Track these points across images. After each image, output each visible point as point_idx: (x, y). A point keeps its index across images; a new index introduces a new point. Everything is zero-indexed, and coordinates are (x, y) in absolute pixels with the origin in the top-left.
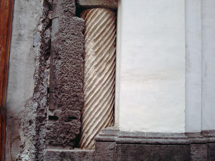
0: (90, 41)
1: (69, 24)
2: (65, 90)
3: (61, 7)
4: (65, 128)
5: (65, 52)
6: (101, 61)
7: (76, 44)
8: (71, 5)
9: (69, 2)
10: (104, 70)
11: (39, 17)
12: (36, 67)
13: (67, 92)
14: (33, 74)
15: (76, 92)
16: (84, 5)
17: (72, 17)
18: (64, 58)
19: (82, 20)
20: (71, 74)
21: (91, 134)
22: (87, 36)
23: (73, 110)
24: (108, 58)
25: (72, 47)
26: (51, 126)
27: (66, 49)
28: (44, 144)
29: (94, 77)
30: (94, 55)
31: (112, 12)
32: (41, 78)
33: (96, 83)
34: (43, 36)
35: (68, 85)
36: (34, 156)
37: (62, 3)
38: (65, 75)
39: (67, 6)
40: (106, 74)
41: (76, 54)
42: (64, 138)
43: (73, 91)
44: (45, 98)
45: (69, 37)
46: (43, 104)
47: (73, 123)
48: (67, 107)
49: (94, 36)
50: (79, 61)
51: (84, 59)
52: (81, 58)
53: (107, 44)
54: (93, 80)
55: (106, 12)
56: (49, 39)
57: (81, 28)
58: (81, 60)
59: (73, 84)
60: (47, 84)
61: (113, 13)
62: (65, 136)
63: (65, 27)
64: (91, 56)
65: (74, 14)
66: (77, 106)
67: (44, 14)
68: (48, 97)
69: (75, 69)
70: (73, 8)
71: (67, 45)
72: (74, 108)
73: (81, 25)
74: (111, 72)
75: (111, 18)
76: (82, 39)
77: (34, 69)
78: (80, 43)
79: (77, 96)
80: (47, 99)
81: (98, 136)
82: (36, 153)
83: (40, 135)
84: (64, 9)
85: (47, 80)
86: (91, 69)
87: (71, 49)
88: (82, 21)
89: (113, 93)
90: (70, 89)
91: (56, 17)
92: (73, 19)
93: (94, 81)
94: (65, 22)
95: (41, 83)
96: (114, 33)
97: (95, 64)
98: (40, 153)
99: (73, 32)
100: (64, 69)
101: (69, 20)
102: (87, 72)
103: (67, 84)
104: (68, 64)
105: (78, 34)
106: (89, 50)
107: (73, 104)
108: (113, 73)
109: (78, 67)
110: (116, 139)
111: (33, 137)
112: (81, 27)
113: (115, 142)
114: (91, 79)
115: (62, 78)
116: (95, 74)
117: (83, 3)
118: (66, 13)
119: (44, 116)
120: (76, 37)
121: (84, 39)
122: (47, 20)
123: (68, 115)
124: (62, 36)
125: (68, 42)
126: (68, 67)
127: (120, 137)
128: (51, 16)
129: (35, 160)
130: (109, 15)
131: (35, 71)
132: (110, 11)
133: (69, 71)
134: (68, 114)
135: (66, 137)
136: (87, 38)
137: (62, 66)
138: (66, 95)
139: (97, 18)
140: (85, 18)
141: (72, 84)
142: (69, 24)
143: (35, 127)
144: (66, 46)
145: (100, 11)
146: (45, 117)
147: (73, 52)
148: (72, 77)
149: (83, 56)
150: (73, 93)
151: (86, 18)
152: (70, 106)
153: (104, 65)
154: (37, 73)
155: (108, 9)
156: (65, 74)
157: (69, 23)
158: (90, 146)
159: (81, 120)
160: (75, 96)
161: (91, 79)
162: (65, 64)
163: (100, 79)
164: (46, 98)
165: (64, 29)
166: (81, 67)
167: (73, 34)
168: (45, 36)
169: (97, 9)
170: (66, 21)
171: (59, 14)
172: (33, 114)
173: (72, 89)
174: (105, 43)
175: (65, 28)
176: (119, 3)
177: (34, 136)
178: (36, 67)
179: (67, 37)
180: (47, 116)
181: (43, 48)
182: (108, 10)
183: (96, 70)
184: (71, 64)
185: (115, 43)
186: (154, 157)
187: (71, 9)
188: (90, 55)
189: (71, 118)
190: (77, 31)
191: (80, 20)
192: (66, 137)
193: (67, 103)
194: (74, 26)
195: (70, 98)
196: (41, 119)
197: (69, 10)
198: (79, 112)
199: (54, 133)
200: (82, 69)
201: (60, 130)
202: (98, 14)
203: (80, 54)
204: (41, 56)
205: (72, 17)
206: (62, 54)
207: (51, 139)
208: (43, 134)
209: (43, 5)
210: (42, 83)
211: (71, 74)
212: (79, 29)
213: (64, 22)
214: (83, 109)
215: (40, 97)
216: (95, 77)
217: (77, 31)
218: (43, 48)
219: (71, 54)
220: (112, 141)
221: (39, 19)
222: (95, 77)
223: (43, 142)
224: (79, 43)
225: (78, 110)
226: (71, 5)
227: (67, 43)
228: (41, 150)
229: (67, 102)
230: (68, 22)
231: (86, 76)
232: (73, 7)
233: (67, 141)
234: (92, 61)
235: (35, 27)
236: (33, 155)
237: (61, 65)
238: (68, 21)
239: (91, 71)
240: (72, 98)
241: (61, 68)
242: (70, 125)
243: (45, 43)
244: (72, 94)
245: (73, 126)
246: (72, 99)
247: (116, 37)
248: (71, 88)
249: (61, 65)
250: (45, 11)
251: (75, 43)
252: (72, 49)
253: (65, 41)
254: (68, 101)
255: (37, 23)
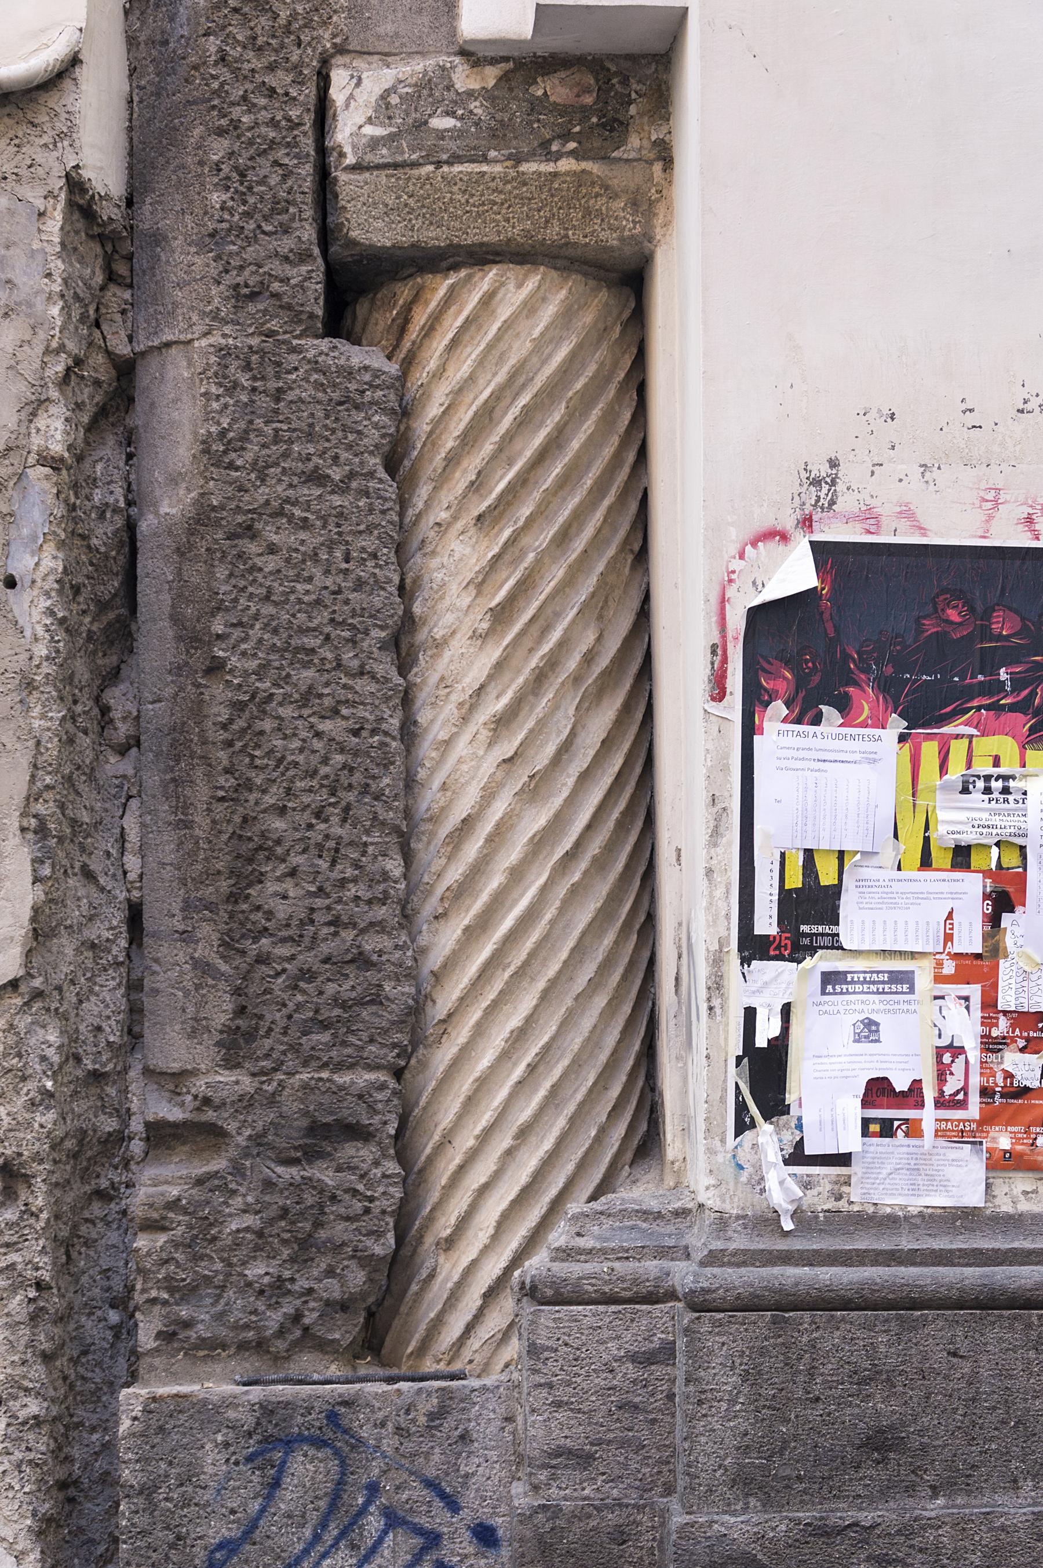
0: (449, 525)
1: (278, 395)
2: (269, 915)
3: (202, 263)
4: (285, 1211)
5: (256, 617)
6: (540, 678)
7: (338, 554)
8: (286, 244)
9: (266, 218)
10: (566, 748)
11: (39, 349)
12: (38, 743)
13: (284, 933)
14: (19, 799)
15: (354, 925)
16: (388, 244)
17: (295, 342)
18: (253, 664)
19: (376, 365)
20: (310, 790)
21: (486, 1250)
22: (424, 491)
23: (340, 1067)
24: (589, 658)
25: (310, 579)
26: (173, 1205)
27: (267, 598)
28: (112, 1345)
29: (489, 805)
30: (482, 638)
31: (603, 295)
32: (74, 822)
33: (512, 855)
34: (72, 499)
35: (293, 873)
36: (41, 1443)
37: (211, 226)
38: (269, 800)
39: (251, 253)
40: (585, 777)
41: (347, 634)
42: (279, 1287)
43: (329, 924)
44: (112, 984)
45: (287, 500)
46: (99, 1029)
47: (339, 1170)
48: (294, 1048)
49: (477, 486)
50: (372, 687)
51: (403, 669)
52: (385, 666)
53: (579, 544)
54: (486, 827)
55: (564, 292)
56: (119, 521)
57: (376, 426)
58: (387, 680)
59: (334, 863)
60: (125, 873)
61: (612, 302)
62: (287, 1274)
63: (251, 422)
64: (459, 645)
65: (312, 316)
66: (372, 1041)
67: (76, 315)
68: (133, 976)
69: (342, 751)
70: (304, 269)
71: (271, 563)
72: (349, 1051)
73: (377, 403)
74: (617, 762)
75: (600, 340)
76: (383, 512)
77: (24, 761)
78: (369, 543)
79: (362, 961)
80: (127, 995)
81: (537, 1263)
82: (55, 1419)
83: (85, 1279)
84: (228, 280)
85: (122, 838)
86: (461, 748)
87: (306, 599)
88: (377, 373)
89: (637, 927)
90: (312, 910)
91: (168, 345)
92: (310, 355)
93: (490, 840)
94: (244, 380)
95: (77, 865)
96: (631, 457)
97: (496, 705)
98: (81, 1424)
99: (311, 465)
100: (257, 753)
101: (279, 364)
102: (433, 771)
103: (282, 869)
104: (287, 712)
105: (352, 475)
106: (442, 598)
107: (339, 1020)
108: (638, 770)
109: (364, 733)
110: (684, 1275)
111: (32, 1293)
112: (376, 418)
113: (680, 1305)
114: (468, 824)
115: (245, 820)
116: (501, 785)
117: (380, 224)
118: (251, 308)
119: (109, 1124)
120: (337, 500)
121: (401, 515)
122: (98, 366)
123: (306, 1113)
124: (230, 491)
125: (275, 538)
126: (285, 737)
127: (713, 1258)
128: (123, 334)
129: (49, 1473)
130: (588, 318)
131: (33, 776)
132: (592, 283)
133: (296, 764)
134: (302, 1101)
135: (296, 1287)
136: (421, 505)
137: (244, 731)
138: (284, 951)
139: (603, 673)
140: (396, 346)
141: (323, 865)
142: (278, 395)
143: (44, 1216)
144: (260, 570)
145: (514, 290)
146: (120, 1138)
147: (321, 617)
148: (318, 815)
149: (404, 643)
150: (338, 940)
151: (406, 344)
152: (315, 1037)
153: (560, 714)
154: (48, 787)
155: (577, 271)
156: (264, 792)
157: (279, 390)
158: (477, 1345)
159: (402, 1143)
160: (352, 961)
161: (468, 824)
162: (264, 712)
163: (537, 820)
164: (119, 985)
165: (244, 437)
166: (386, 734)
167: (317, 478)
168: (88, 498)
169: (493, 272)
170: (254, 378)
171: (195, 318)
172: (28, 1116)
173: (329, 908)
174: (563, 537)
175: (246, 432)
176: (658, 221)
177: (39, 1285)
178: (38, 743)
179: (267, 503)
180: (136, 1125)
181: (76, 590)
182: (579, 277)
183: (507, 748)
184: (306, 712)
185: (640, 536)
186: (974, 1400)
187: (285, 280)
188: (454, 633)
189: (329, 1133)
190: (344, 455)
191: (366, 368)
192: (292, 1280)
193: (290, 1017)
194: (321, 414)
195: (307, 974)
196: (89, 1153)
197: (276, 286)
198: (382, 1087)
199: (197, 1258)
200: (394, 744)
201: (247, 1229)
202: (504, 313)
203: (376, 633)
204: (71, 656)
205: (295, 342)
206: (237, 633)
207: (177, 1304)
208: (106, 1272)
209: (63, 244)
210: (84, 868)
211: (310, 790)
212: (359, 433)
213: (236, 385)
214: (413, 1061)
215: (80, 973)
216: (499, 809)
217: (344, 455)
218: (76, 590)
219: (303, 631)
220: (651, 1298)
221: (37, 364)
222: (499, 809)
223: (109, 1335)
224: (363, 549)
225: (378, 1067)
226: (286, 244)
227: (272, 549)
228: (92, 1393)
229: (291, 1005)
230: (273, 385)
231: (429, 798)
232: (304, 257)
233: (297, 1317)
234: (467, 680)
235: (12, 424)
236: (31, 1436)
237: (231, 721)
238: (270, 371)
239: (464, 765)
240: (329, 980)
241: (229, 744)
242: (320, 1189)
243: (89, 547)
244: (325, 948)
245: (347, 1197)
246: (331, 988)
247: (646, 489)
248: (319, 902)
249: (231, 721)
250: (77, 297)
251: (330, 545)
252: (307, 592)
253: (249, 531)
254: (300, 998)
255: (21, 389)
